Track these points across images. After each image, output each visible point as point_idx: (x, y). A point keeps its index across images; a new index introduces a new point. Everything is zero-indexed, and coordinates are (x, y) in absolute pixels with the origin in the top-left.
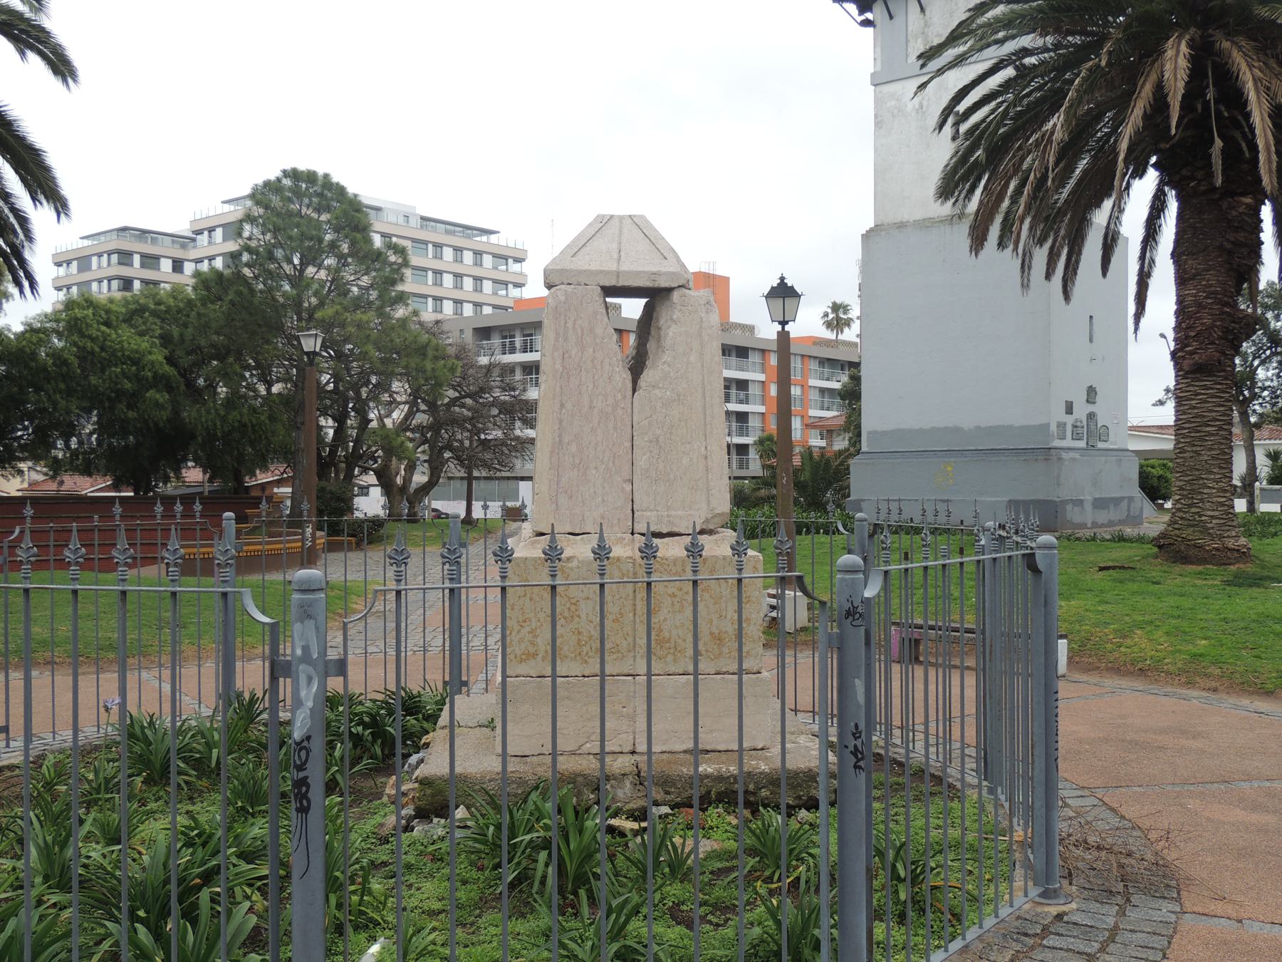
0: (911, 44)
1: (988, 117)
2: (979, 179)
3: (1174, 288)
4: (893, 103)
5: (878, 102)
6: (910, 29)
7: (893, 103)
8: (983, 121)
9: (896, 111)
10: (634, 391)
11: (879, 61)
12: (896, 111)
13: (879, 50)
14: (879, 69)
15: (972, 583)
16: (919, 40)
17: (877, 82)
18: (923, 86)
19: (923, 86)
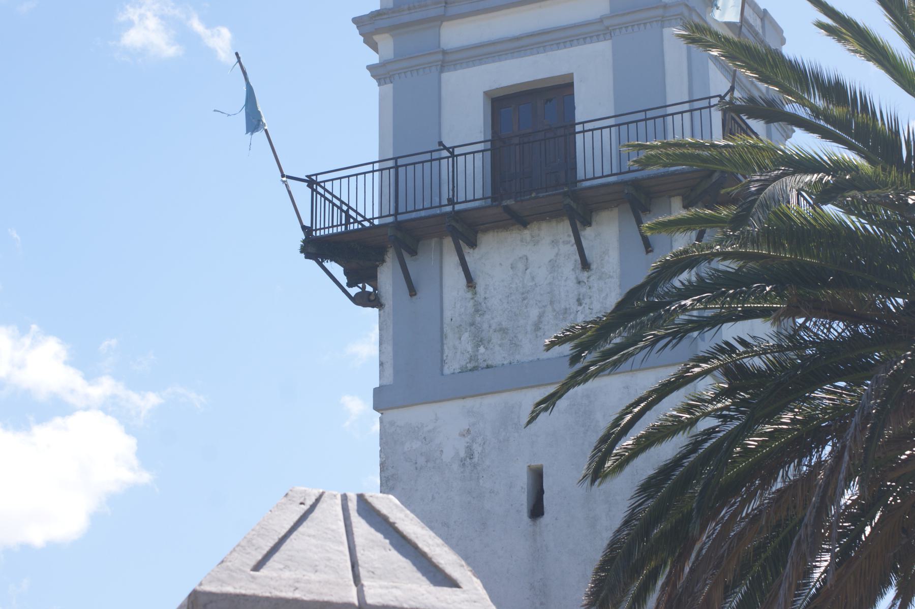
0: (450, 341)
1: (685, 456)
2: (653, 576)
3: (367, 12)
4: (416, 445)
5: (388, 440)
6: (448, 314)
7: (416, 445)
8: (677, 462)
9: (421, 461)
10: (529, 422)
11: (389, 371)
12: (421, 461)
13: (389, 348)
14: (389, 380)
15: (694, 279)
16: (466, 336)
17: (383, 400)
18: (549, 402)
19: (549, 402)
